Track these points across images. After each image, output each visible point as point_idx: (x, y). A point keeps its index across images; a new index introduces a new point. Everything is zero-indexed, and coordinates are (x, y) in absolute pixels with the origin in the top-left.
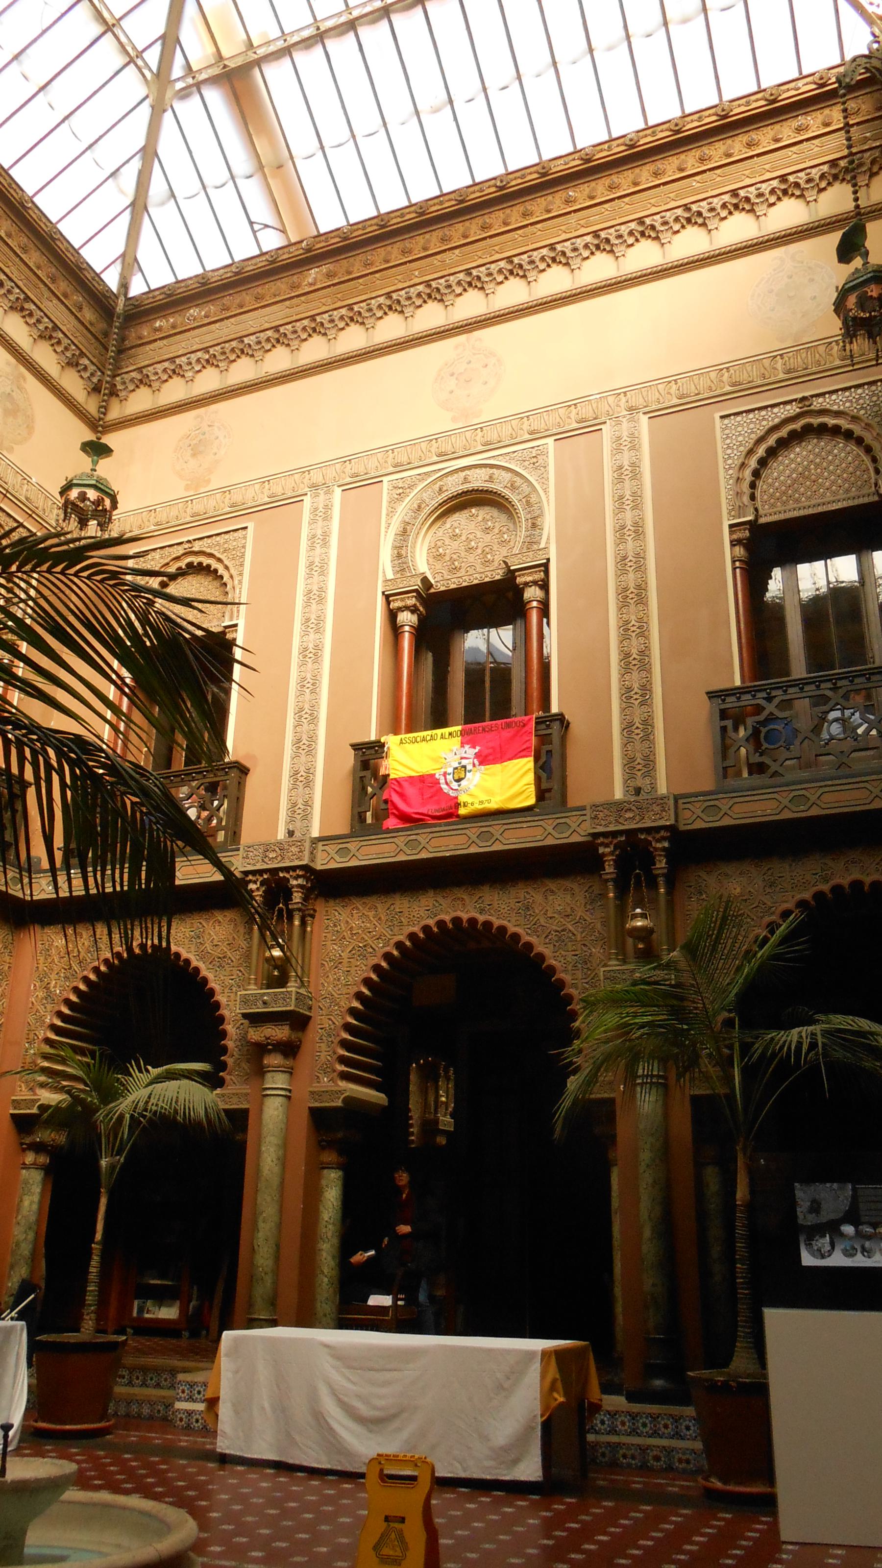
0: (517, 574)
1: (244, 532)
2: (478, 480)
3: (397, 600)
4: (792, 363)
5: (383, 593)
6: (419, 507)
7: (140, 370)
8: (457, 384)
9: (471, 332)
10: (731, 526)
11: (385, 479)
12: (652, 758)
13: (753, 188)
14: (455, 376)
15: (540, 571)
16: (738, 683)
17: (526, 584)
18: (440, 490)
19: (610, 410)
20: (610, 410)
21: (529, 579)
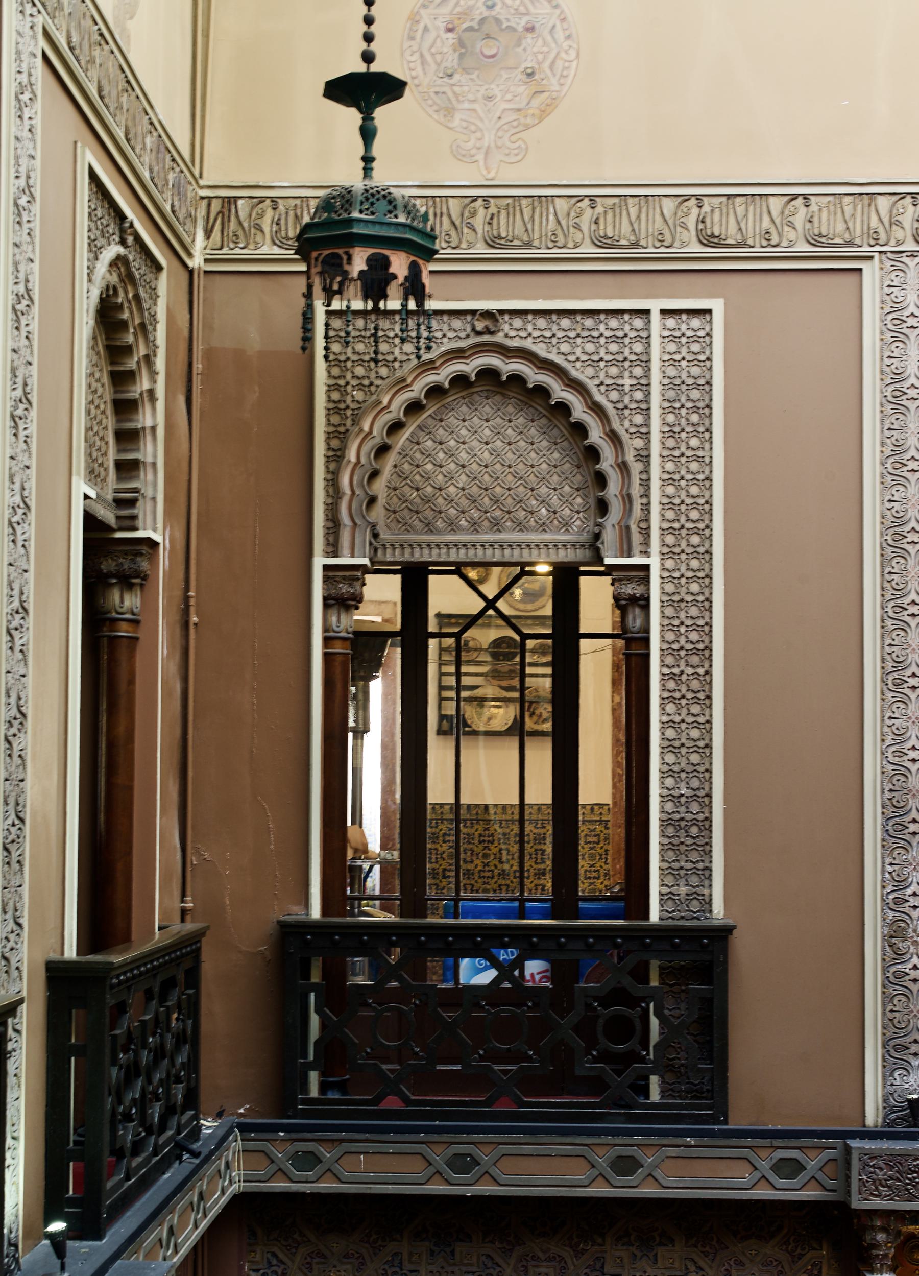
1: (638, 323)
10: (326, 568)
20: (666, 232)
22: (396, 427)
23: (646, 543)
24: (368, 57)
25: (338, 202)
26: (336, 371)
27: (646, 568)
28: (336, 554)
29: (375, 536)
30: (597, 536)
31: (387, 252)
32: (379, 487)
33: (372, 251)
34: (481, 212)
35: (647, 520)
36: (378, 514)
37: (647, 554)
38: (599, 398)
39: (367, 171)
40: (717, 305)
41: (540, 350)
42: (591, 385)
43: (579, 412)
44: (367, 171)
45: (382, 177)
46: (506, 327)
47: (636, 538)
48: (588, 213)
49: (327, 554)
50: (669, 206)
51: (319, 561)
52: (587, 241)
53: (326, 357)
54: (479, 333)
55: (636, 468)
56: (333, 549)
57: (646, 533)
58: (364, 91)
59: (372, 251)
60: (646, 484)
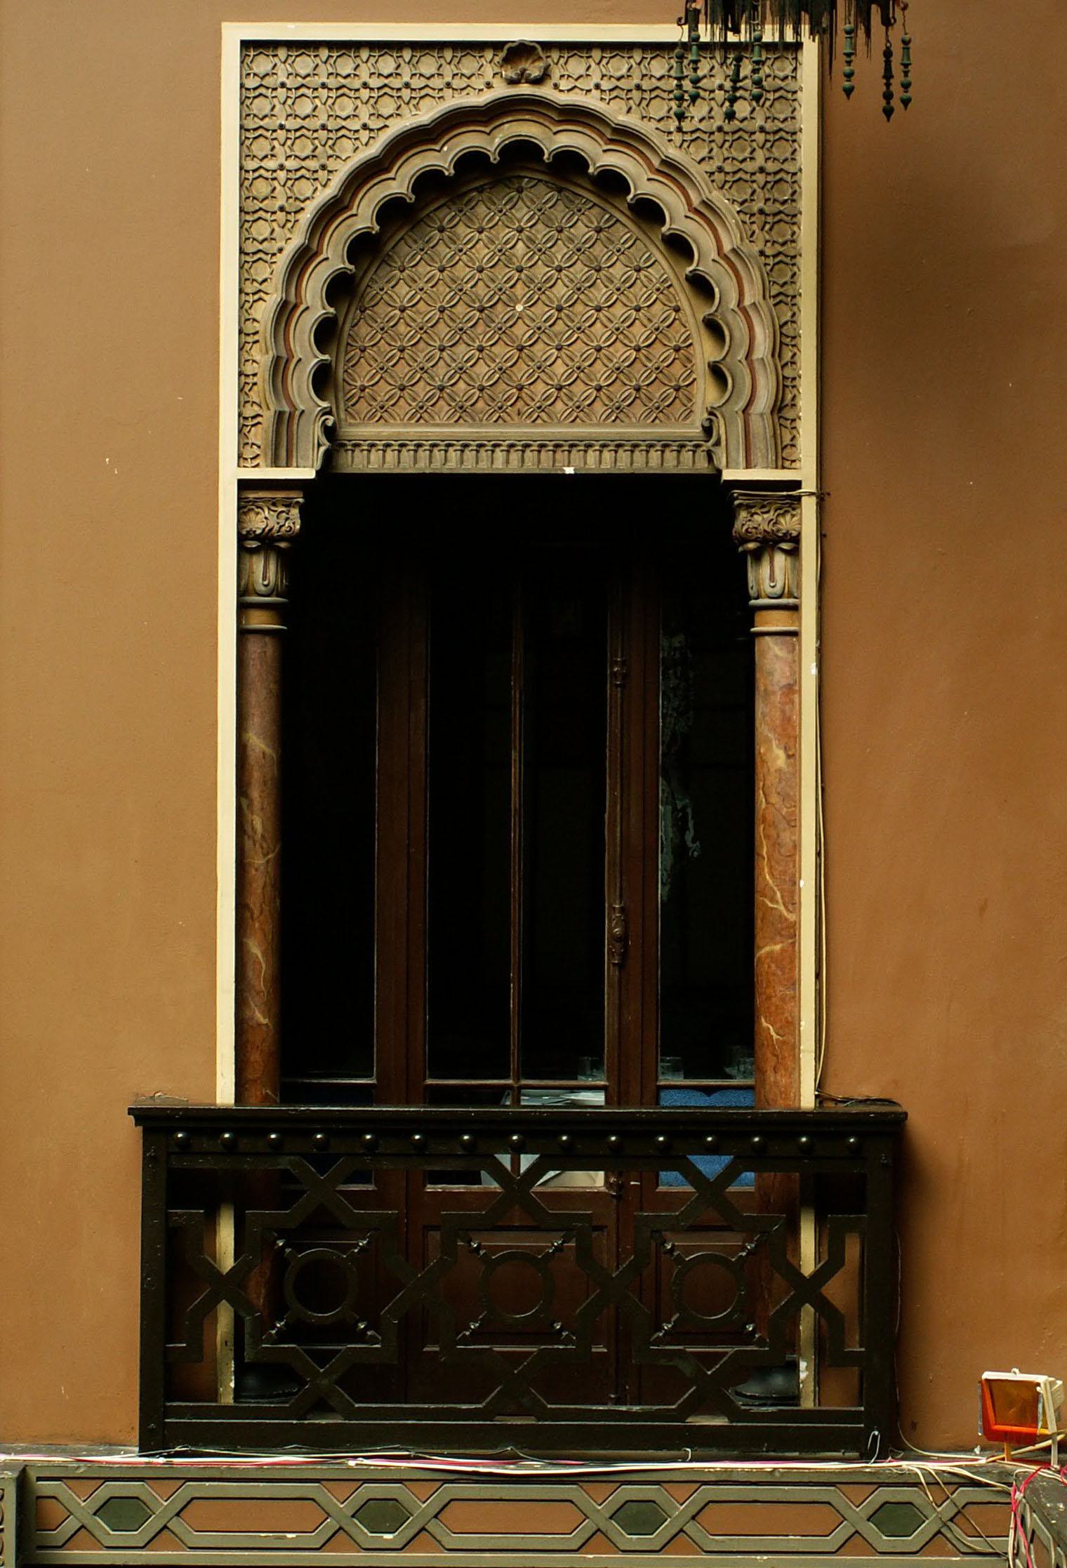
15: (288, 504)
16: (225, 1095)
27: (797, 484)
37: (781, 461)
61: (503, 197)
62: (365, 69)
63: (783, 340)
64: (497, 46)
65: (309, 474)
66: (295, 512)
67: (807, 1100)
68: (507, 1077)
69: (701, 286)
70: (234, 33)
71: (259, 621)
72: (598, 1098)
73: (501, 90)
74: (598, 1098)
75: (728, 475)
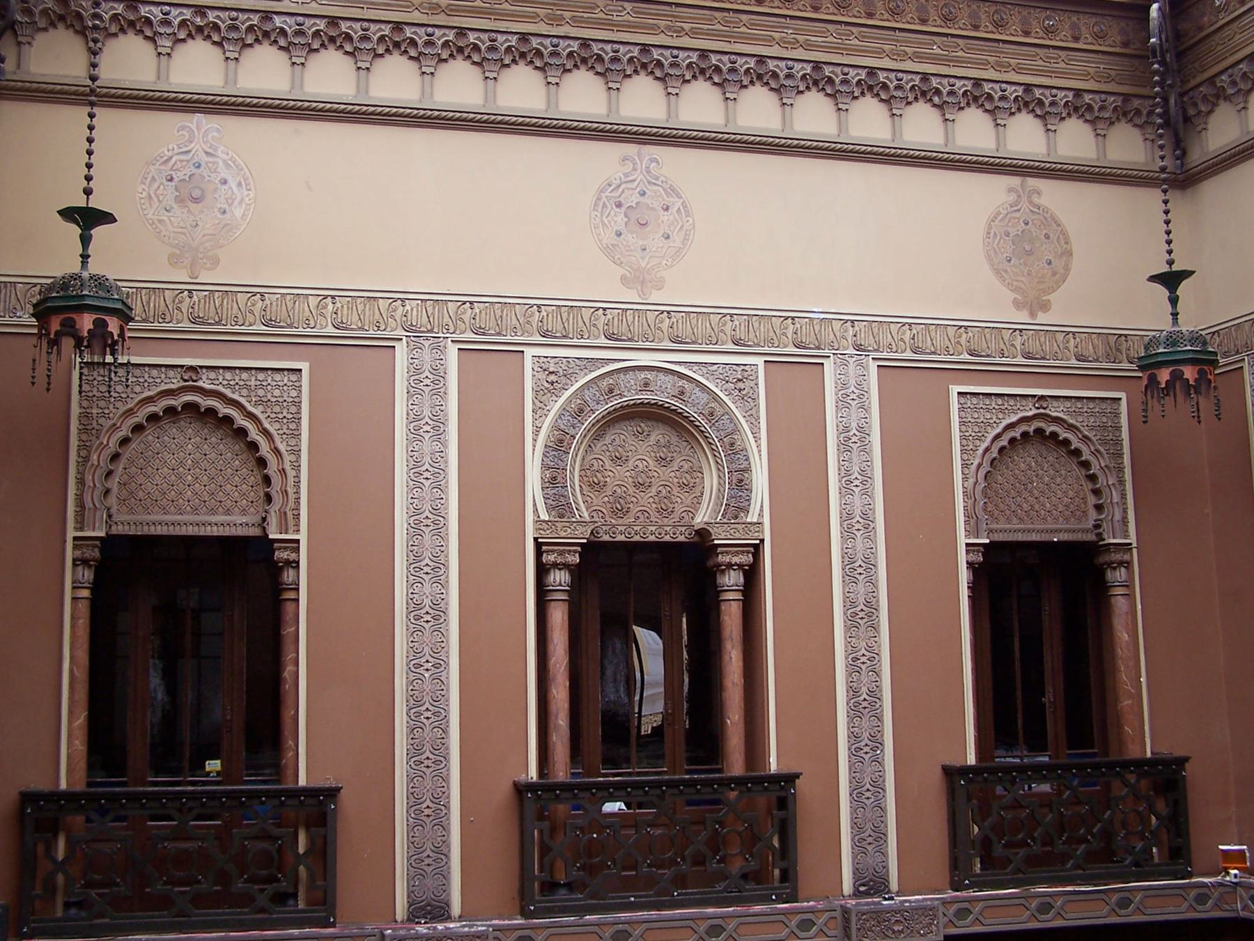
0: (276, 545)
1: (294, 377)
2: (663, 392)
3: (553, 551)
4: (1033, 346)
5: (536, 539)
6: (581, 411)
7: (1211, 81)
8: (626, 224)
9: (645, 144)
10: (75, 539)
11: (529, 352)
12: (445, 851)
13: (423, 30)
14: (623, 209)
15: (748, 552)
16: (971, 759)
17: (730, 566)
18: (611, 391)
19: (239, 315)
20: (239, 315)
21: (736, 560)
22: (125, 441)
23: (297, 525)
24: (1170, 263)
25: (65, 284)
26: (85, 404)
27: (298, 541)
28: (81, 529)
29: (110, 516)
30: (264, 519)
31: (107, 318)
32: (113, 484)
33: (95, 316)
34: (964, 335)
35: (298, 509)
36: (112, 500)
37: (1126, 537)
38: (267, 425)
39: (84, 263)
40: (304, 366)
41: (228, 392)
42: (262, 417)
43: (254, 434)
44: (84, 263)
45: (94, 267)
46: (204, 377)
47: (291, 522)
48: (964, 335)
49: (76, 529)
50: (837, 325)
51: (71, 533)
52: (258, 321)
53: (80, 392)
54: (186, 381)
55: (291, 474)
56: (80, 525)
57: (297, 517)
58: (1171, 280)
59: (95, 316)
60: (297, 484)
61: (197, 425)
62: (994, 403)
63: (1123, 496)
64: (182, 366)
65: (102, 534)
66: (97, 550)
67: (1149, 754)
68: (1092, 747)
69: (1092, 478)
70: (955, 389)
71: (292, 595)
72: (1047, 759)
73: (1034, 412)
74: (1047, 759)
75: (271, 537)
